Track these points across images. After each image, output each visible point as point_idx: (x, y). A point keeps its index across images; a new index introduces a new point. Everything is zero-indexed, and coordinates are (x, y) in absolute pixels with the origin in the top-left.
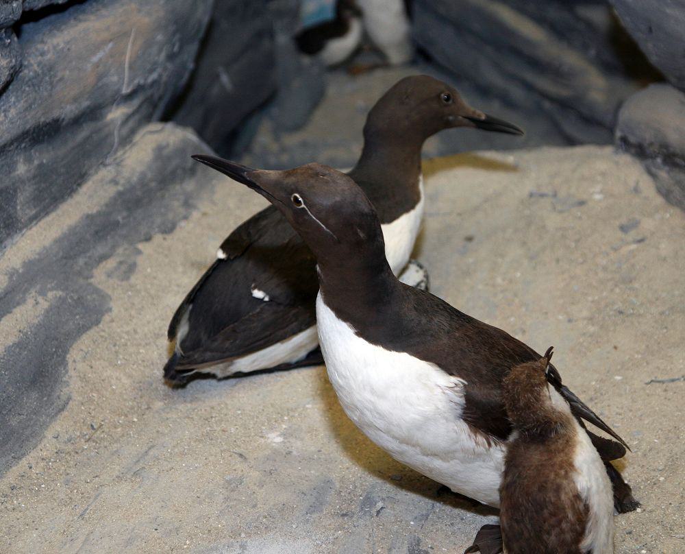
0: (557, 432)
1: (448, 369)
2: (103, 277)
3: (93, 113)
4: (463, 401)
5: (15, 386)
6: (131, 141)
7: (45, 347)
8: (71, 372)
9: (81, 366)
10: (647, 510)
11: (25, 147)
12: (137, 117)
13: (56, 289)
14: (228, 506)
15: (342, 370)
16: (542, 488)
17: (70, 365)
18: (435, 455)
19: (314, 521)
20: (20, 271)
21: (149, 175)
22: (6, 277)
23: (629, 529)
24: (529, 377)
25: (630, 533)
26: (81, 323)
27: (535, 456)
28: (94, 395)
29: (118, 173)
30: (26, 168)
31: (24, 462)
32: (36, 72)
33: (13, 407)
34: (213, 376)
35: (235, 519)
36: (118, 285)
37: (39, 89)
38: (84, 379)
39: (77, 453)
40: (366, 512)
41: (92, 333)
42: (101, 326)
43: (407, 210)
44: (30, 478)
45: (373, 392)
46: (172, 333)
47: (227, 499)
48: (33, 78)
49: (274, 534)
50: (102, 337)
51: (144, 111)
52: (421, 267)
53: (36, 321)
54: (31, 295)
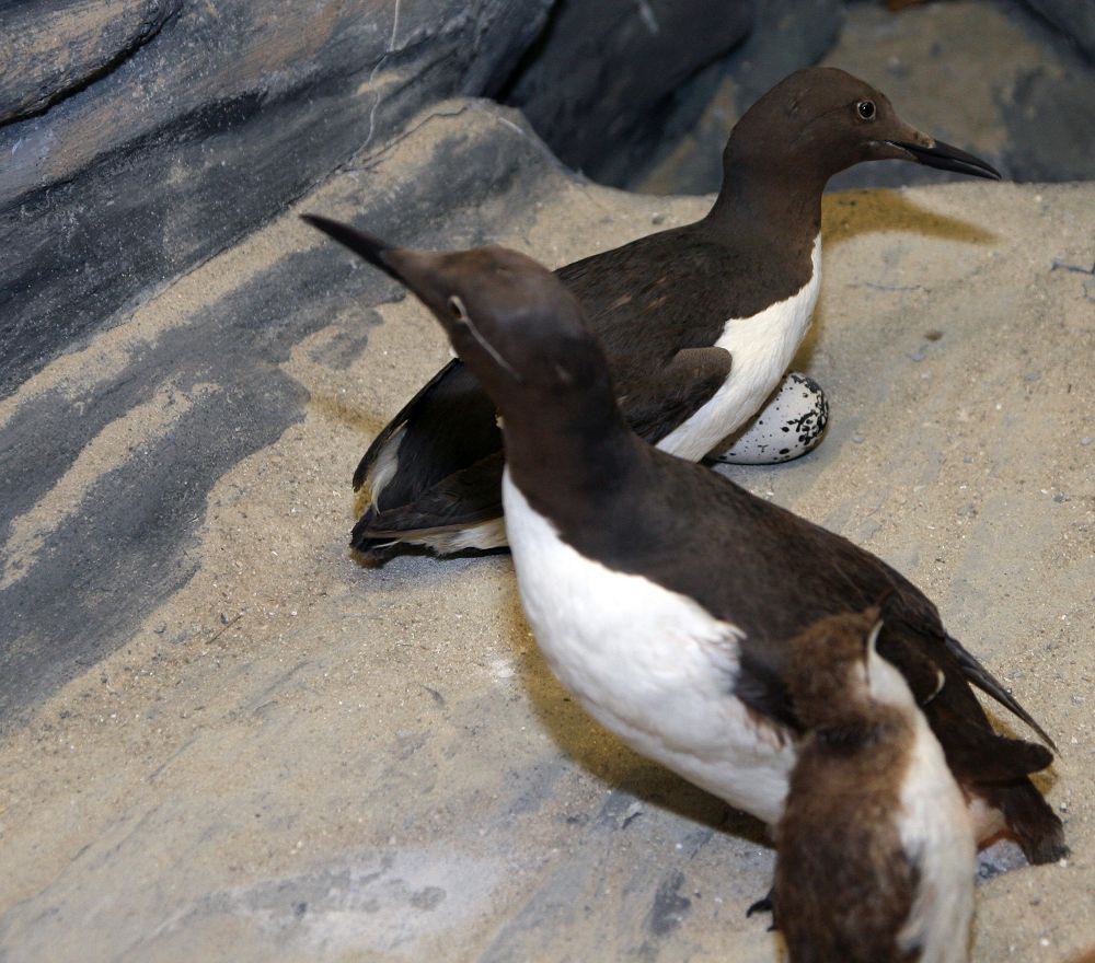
0: (877, 740)
1: (717, 613)
2: (306, 361)
3: (331, 82)
4: (734, 666)
5: (102, 541)
6: (401, 131)
7: (170, 478)
8: (210, 523)
9: (227, 513)
10: (1078, 863)
11: (186, 140)
12: (418, 88)
13: (210, 381)
14: (386, 785)
15: (535, 594)
16: (839, 835)
17: (211, 511)
18: (688, 751)
19: (520, 826)
20: (154, 346)
21: (419, 190)
22: (127, 355)
23: (1036, 895)
24: (833, 643)
25: (1036, 903)
26: (242, 439)
27: (835, 779)
28: (239, 563)
29: (365, 183)
30: (186, 174)
31: (95, 672)
32: (210, 15)
33: (94, 577)
34: (429, 552)
35: (389, 811)
36: (327, 376)
37: (216, 45)
38: (228, 535)
39: (187, 662)
40: (607, 818)
41: (259, 458)
42: (277, 445)
43: (782, 296)
44: (98, 700)
45: (581, 637)
46: (360, 477)
47: (389, 771)
48: (205, 27)
49: (446, 843)
50: (275, 464)
51: (434, 77)
52: (813, 387)
53: (161, 434)
54: (165, 388)
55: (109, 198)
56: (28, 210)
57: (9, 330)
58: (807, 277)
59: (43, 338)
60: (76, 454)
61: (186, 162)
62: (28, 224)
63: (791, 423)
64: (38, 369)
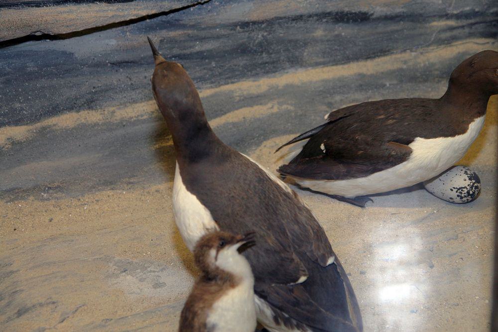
21: (437, 67)
53: (258, 116)
55: (280, 33)
56: (240, 28)
57: (222, 66)
58: (463, 131)
59: (237, 73)
60: (225, 113)
61: (325, 30)
62: (239, 33)
63: (454, 188)
64: (233, 83)
